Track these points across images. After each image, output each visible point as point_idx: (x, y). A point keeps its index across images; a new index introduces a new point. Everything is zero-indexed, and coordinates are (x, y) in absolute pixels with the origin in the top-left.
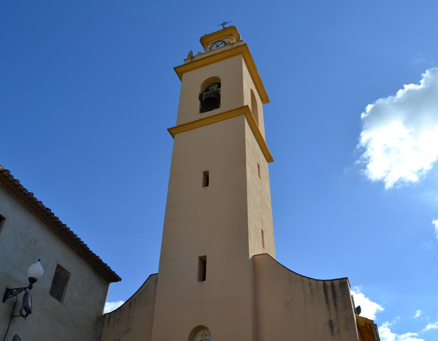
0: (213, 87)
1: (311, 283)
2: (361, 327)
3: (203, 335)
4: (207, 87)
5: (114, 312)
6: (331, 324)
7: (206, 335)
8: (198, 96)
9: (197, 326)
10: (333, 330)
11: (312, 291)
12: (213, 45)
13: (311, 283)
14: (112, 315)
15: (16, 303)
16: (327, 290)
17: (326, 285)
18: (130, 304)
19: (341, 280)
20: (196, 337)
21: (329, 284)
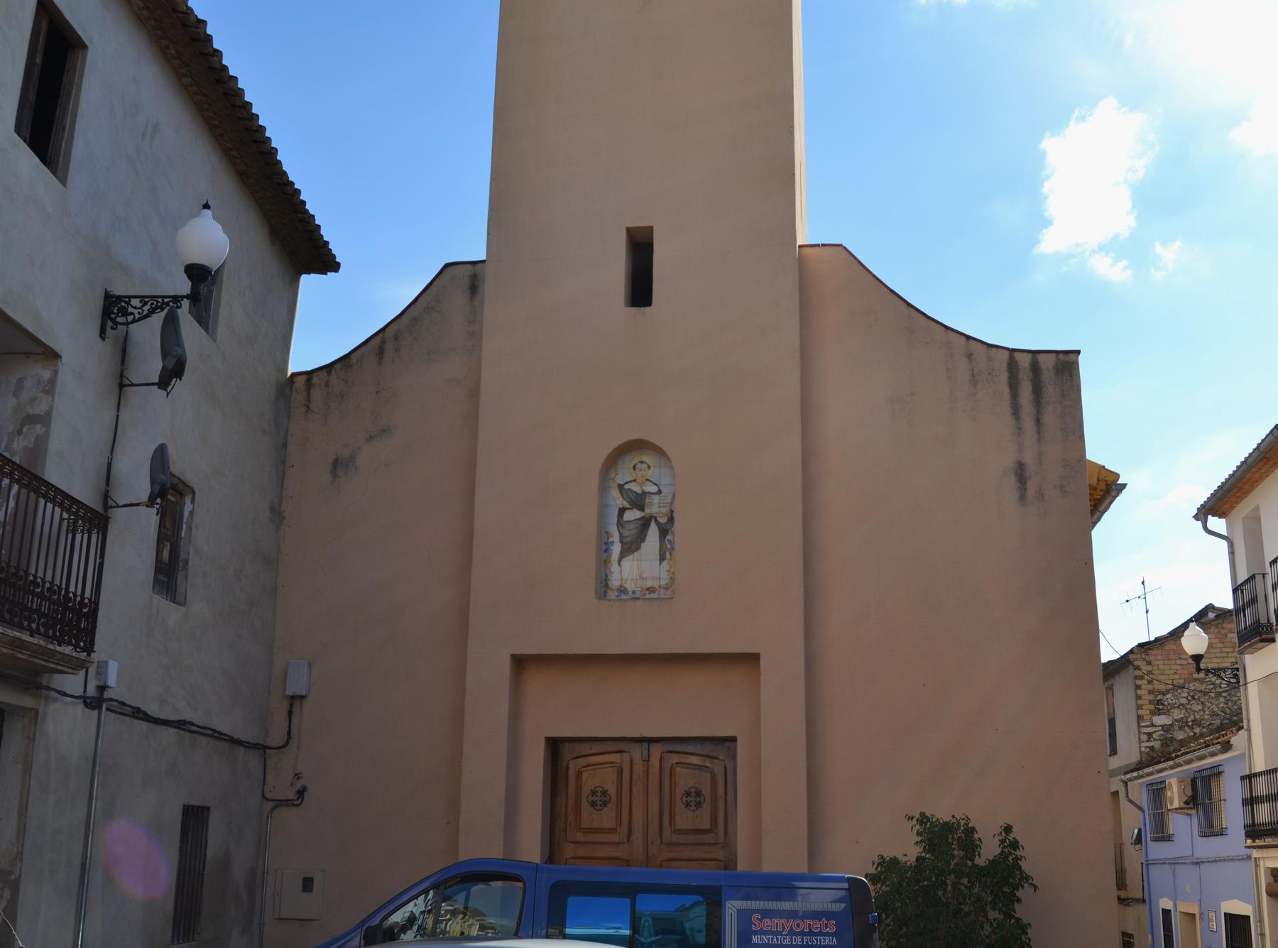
1: (973, 354)
3: (639, 466)
7: (649, 467)
10: (1025, 489)
13: (973, 354)
14: (315, 380)
15: (126, 338)
17: (1016, 363)
18: (381, 350)
19: (1061, 356)
21: (1024, 361)
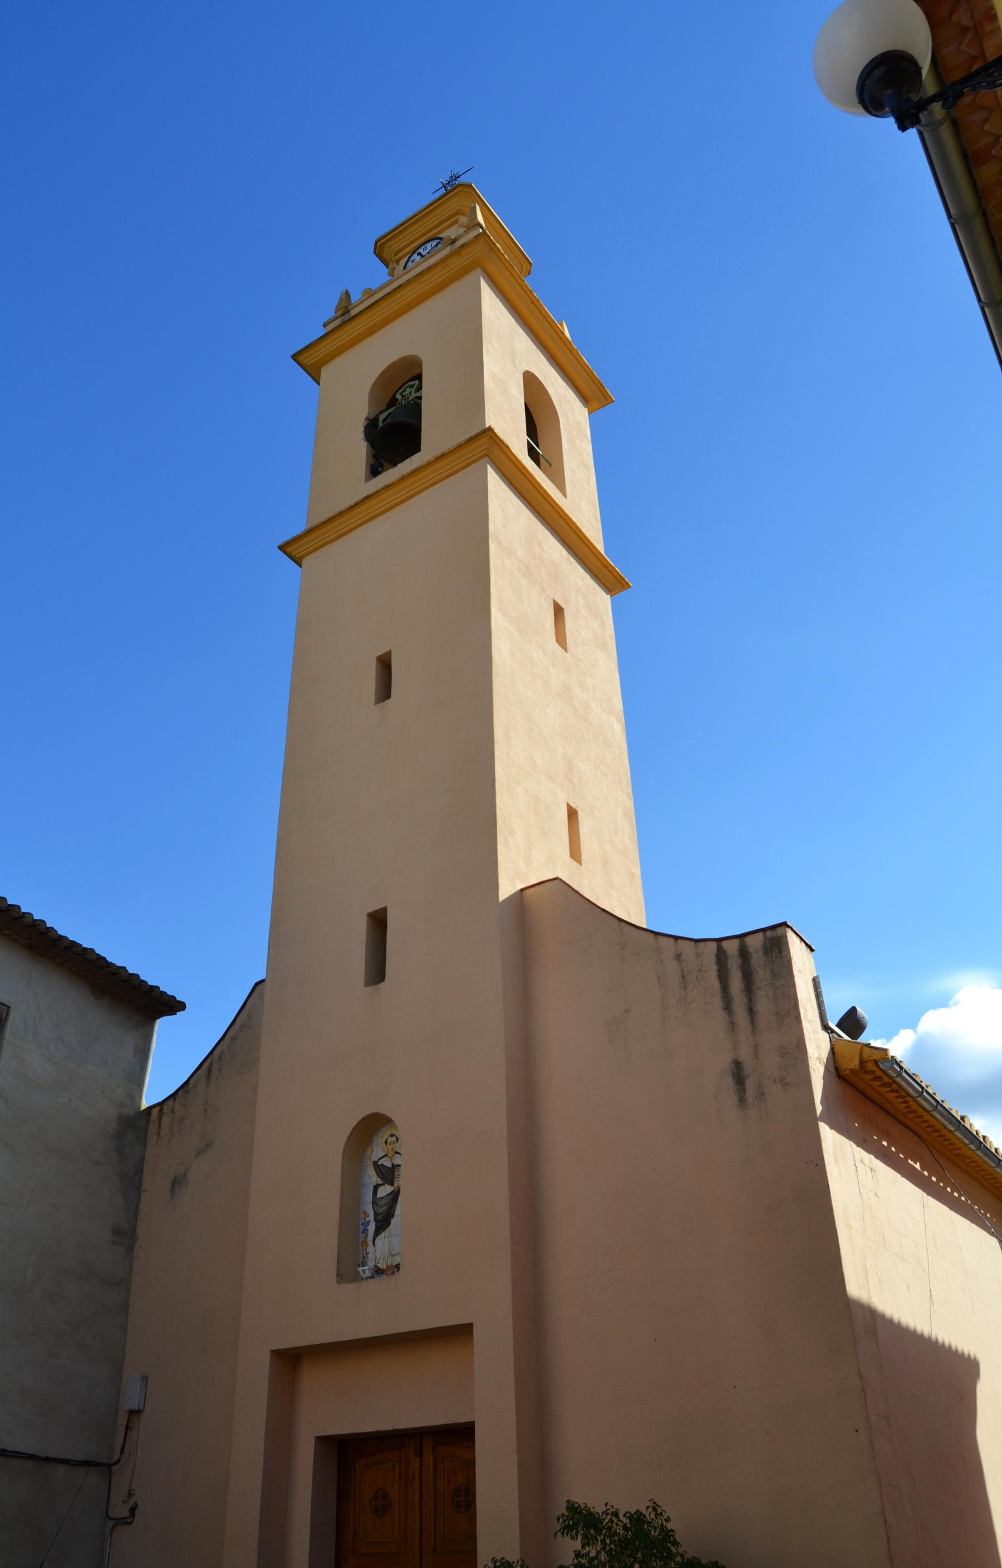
0: (408, 390)
2: (848, 1072)
4: (393, 394)
5: (172, 1099)
6: (738, 1074)
8: (363, 429)
9: (363, 1116)
10: (744, 1090)
11: (683, 976)
12: (410, 257)
16: (727, 969)
17: (725, 952)
18: (209, 1071)
19: (769, 934)
20: (372, 1146)
